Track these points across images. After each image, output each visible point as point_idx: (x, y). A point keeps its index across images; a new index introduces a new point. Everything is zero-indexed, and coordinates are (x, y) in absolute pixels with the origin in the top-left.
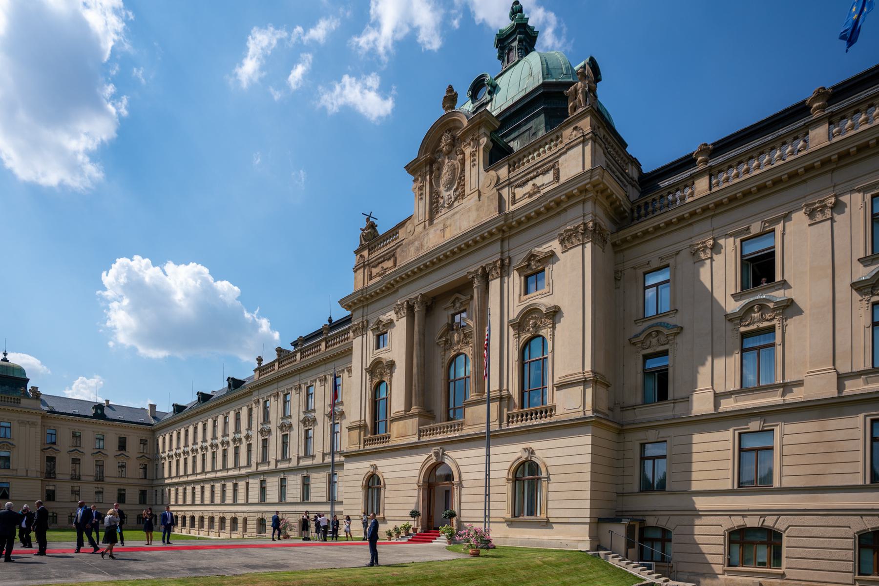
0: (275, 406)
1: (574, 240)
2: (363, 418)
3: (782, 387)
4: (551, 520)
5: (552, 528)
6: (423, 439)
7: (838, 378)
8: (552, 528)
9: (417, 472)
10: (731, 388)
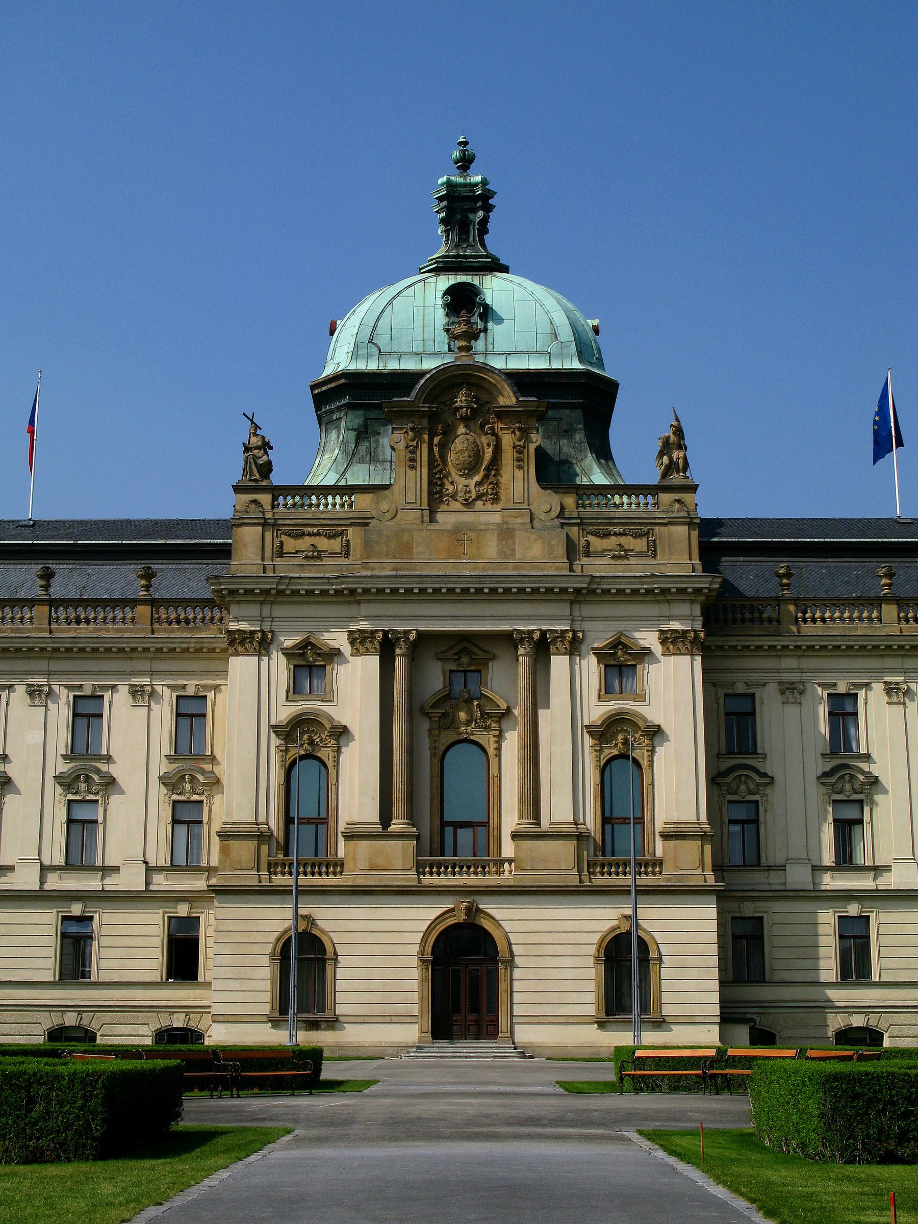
0: (135, 733)
1: (680, 645)
2: (262, 819)
3: (102, 871)
4: (668, 1019)
5: (671, 1030)
6: (427, 880)
7: (41, 869)
8: (671, 1030)
9: (418, 938)
10: (162, 863)
